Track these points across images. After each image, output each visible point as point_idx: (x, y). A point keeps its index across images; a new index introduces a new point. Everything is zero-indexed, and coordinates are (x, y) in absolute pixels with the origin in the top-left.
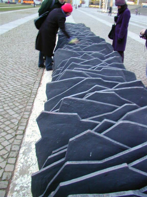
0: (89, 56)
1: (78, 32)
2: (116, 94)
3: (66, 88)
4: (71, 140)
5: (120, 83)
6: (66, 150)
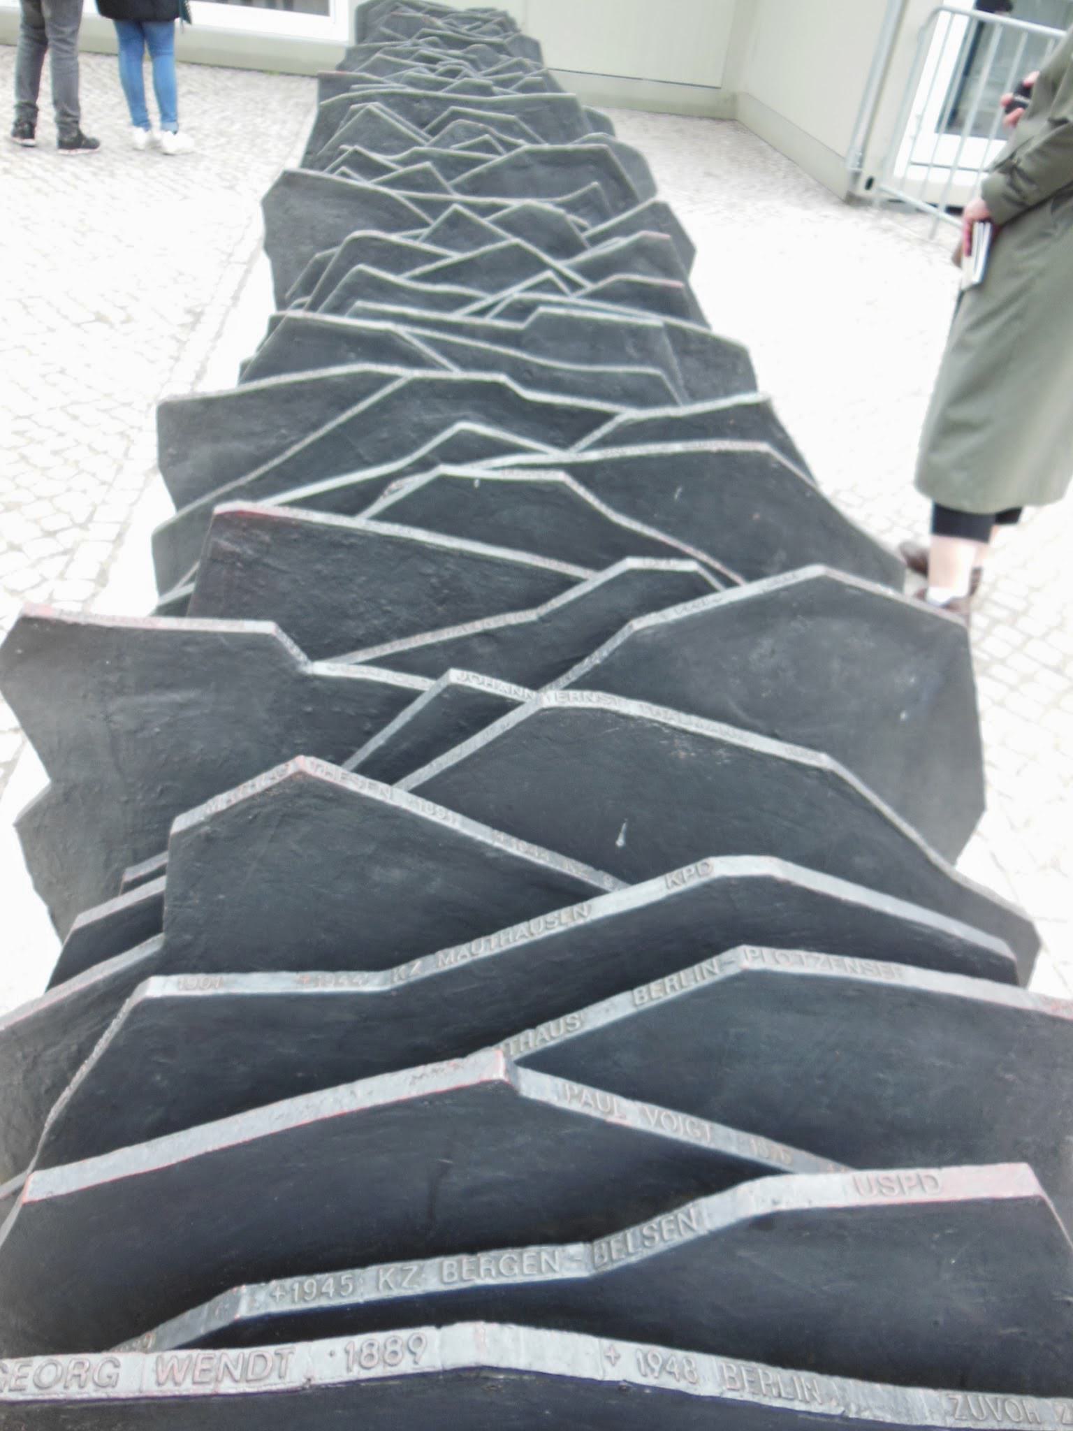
0: (481, 228)
1: (451, 63)
2: (581, 491)
3: (284, 437)
4: (180, 823)
5: (628, 414)
6: (157, 887)
